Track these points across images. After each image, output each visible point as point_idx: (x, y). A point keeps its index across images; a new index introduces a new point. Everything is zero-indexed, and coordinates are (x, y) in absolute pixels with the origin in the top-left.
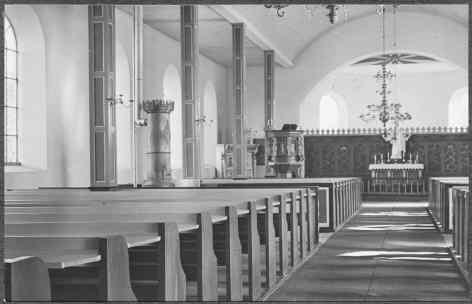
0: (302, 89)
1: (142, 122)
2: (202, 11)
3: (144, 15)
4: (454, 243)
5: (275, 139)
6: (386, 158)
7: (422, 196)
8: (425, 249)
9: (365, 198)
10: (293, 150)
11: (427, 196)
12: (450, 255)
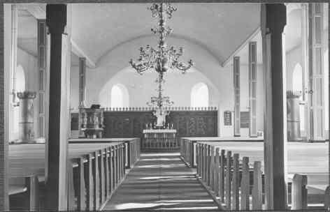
0: (103, 81)
1: (16, 104)
3: (18, 35)
5: (86, 114)
6: (153, 126)
7: (160, 149)
8: (184, 175)
9: (143, 150)
10: (97, 120)
11: (179, 149)
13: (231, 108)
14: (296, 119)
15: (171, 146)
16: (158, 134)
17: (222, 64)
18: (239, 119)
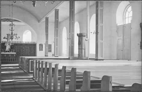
2: (76, 3)
4: (34, 76)
6: (4, 51)
12: (34, 80)
13: (43, 42)
14: (83, 48)
15: (14, 60)
16: (6, 54)
17: (39, 21)
18: (48, 48)
